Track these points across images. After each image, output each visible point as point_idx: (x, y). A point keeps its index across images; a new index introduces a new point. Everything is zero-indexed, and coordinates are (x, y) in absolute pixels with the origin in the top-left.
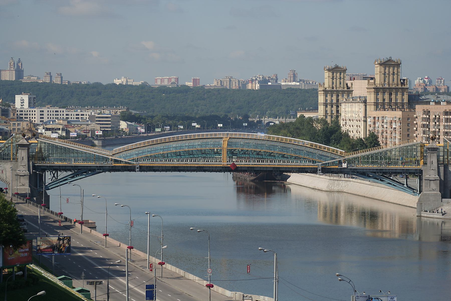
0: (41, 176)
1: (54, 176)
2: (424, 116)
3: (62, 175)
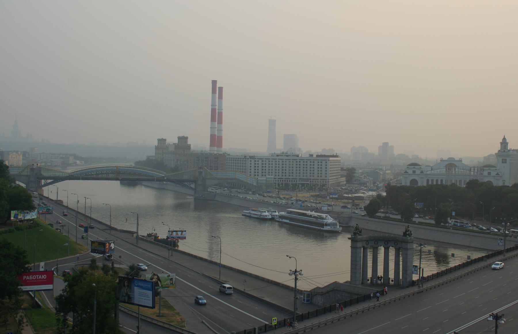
0: (40, 182)
1: (45, 182)
2: (197, 159)
3: (49, 181)
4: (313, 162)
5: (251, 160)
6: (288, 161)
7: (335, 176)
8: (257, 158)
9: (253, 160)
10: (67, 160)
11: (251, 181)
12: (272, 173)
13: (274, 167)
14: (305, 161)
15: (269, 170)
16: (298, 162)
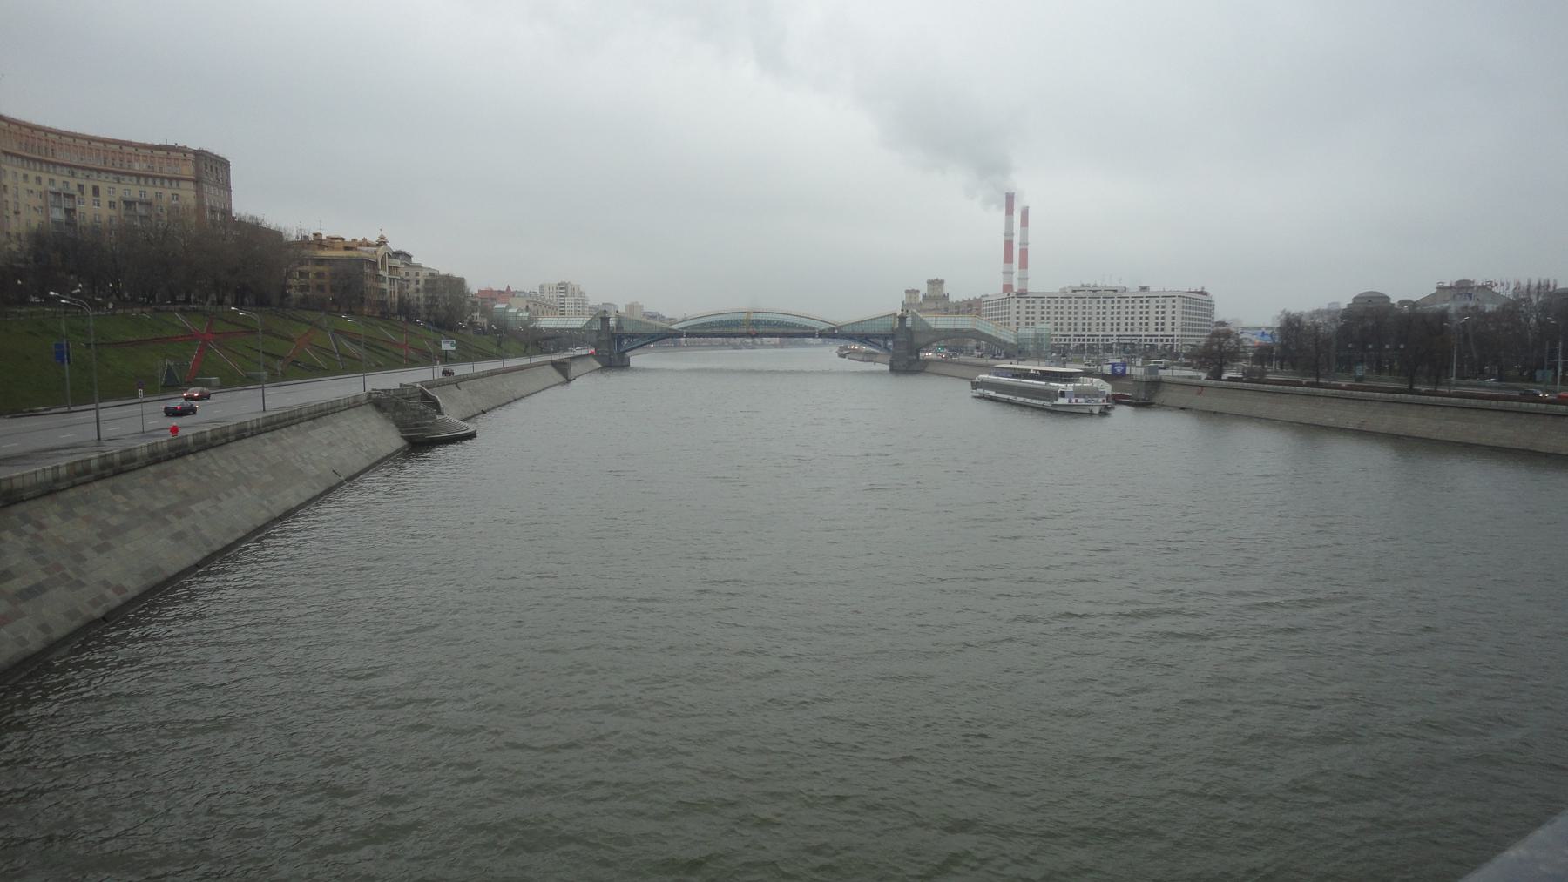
7: (1198, 330)
9: (1023, 301)
10: (1187, 333)
11: (1008, 336)
12: (1048, 318)
13: (1052, 308)
14: (1046, 300)
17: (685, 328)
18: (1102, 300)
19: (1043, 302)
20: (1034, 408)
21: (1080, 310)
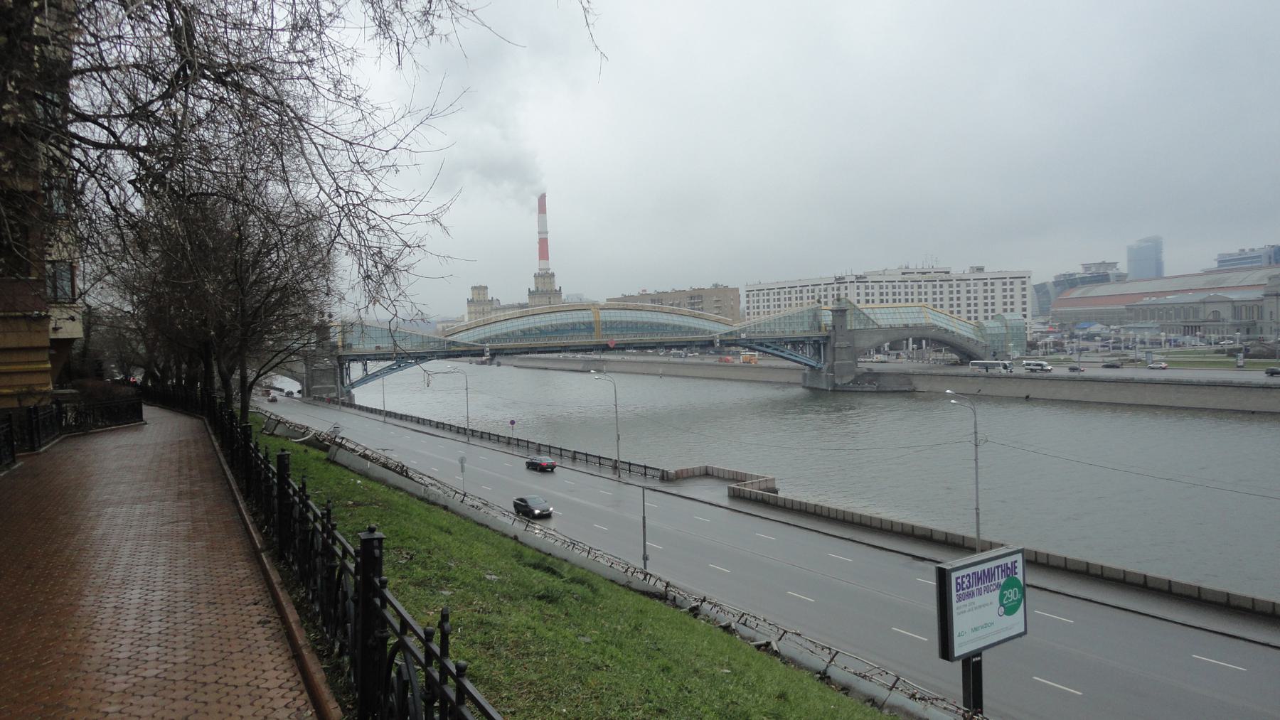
4: (1012, 283)
5: (858, 284)
6: (980, 283)
8: (1008, 277)
9: (862, 286)
14: (1008, 281)
15: (935, 300)
16: (955, 286)
17: (488, 340)
18: (938, 283)
19: (1004, 284)
20: (1154, 408)
21: (964, 295)
